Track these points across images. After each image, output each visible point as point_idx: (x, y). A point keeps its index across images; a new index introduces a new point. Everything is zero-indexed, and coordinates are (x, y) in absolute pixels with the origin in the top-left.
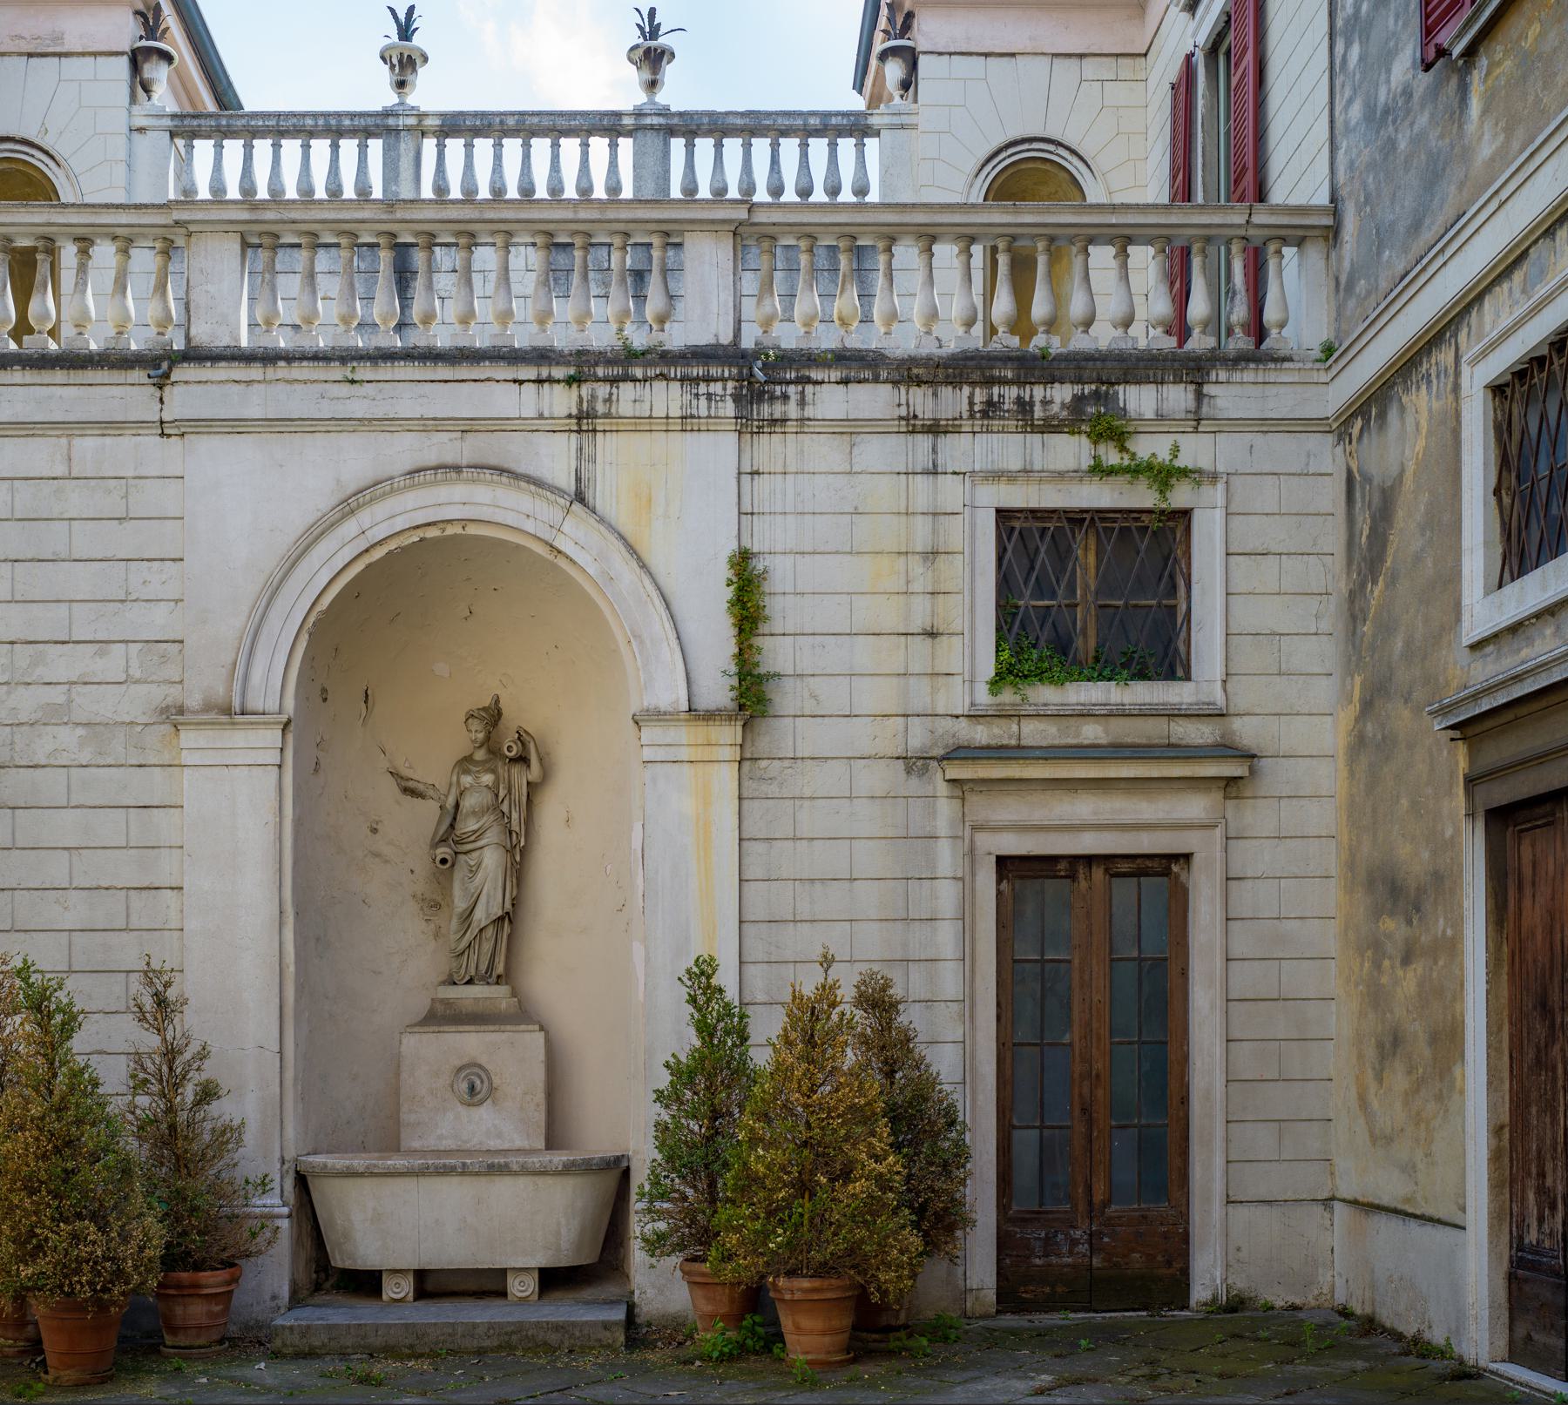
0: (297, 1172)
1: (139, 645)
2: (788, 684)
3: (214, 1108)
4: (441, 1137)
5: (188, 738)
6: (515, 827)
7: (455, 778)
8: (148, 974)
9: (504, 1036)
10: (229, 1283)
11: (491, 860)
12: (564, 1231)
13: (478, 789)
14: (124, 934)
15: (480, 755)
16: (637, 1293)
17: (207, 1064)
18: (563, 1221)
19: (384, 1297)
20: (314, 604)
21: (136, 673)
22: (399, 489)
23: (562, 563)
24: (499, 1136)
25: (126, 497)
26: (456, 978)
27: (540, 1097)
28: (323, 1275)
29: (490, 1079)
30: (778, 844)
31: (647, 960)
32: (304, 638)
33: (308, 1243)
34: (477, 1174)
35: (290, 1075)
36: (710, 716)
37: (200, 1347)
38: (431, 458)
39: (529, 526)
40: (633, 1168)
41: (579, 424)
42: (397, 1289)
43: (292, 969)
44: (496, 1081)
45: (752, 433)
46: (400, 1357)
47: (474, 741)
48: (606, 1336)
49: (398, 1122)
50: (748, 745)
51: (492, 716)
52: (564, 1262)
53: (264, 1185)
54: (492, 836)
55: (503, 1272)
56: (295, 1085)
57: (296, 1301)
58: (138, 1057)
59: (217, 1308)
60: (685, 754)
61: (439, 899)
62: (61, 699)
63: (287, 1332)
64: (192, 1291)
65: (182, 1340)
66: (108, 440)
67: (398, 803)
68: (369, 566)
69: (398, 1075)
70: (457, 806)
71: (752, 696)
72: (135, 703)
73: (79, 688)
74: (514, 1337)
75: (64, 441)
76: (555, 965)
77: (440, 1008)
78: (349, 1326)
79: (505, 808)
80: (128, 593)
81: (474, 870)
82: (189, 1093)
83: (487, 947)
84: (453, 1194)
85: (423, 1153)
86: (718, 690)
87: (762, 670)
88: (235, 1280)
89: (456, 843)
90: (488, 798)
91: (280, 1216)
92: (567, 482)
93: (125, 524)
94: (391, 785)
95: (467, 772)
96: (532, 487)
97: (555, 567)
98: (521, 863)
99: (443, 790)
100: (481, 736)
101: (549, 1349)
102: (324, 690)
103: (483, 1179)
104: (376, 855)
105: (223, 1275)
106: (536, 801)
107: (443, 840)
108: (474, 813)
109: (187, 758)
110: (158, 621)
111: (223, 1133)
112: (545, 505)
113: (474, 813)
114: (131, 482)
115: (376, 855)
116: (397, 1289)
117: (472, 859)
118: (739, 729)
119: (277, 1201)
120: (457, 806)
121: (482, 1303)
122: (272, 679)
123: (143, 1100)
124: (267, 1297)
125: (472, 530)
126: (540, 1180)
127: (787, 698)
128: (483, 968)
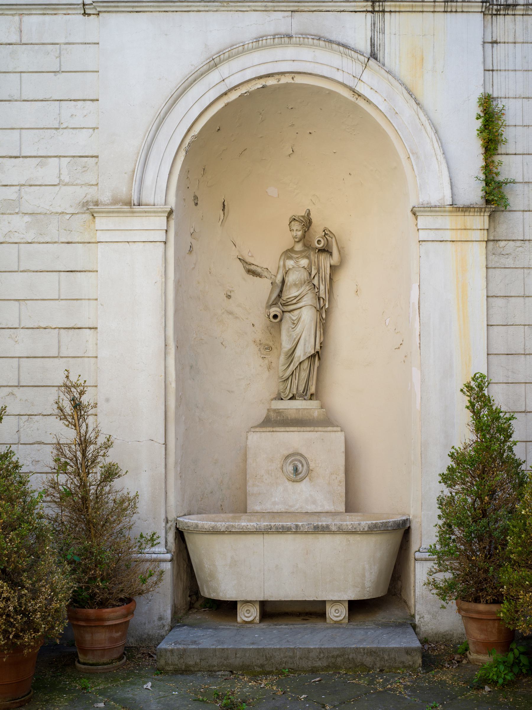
0: (177, 529)
1: (68, 159)
2: (519, 188)
3: (117, 483)
4: (274, 503)
5: (101, 222)
6: (322, 295)
7: (282, 263)
8: (67, 388)
9: (317, 434)
10: (125, 616)
11: (307, 316)
12: (367, 574)
13: (297, 270)
14: (56, 360)
15: (299, 247)
16: (417, 617)
17: (111, 451)
18: (367, 567)
19: (239, 620)
20: (189, 131)
21: (66, 178)
22: (248, 50)
23: (361, 103)
24: (314, 502)
25: (60, 56)
26: (283, 395)
27: (342, 476)
28: (194, 597)
29: (308, 464)
30: (513, 300)
31: (423, 381)
32: (182, 154)
33: (184, 576)
34: (306, 533)
35: (172, 460)
36: (466, 209)
37: (104, 664)
38: (271, 29)
39: (339, 76)
40: (413, 527)
41: (373, 6)
42: (248, 614)
43: (173, 385)
44: (312, 465)
45: (492, 15)
46: (255, 676)
47: (295, 237)
48: (408, 659)
49: (245, 494)
50: (492, 230)
51: (307, 223)
52: (366, 596)
53: (152, 540)
54: (308, 300)
55: (324, 602)
56: (175, 467)
57: (177, 621)
58: (59, 446)
59: (117, 635)
60: (448, 235)
61: (271, 344)
62: (14, 197)
63: (169, 654)
64: (97, 623)
65: (91, 659)
66: (47, 18)
67: (244, 279)
68: (227, 105)
69: (245, 460)
70: (283, 282)
71: (495, 196)
72: (66, 199)
73: (27, 189)
74: (339, 660)
75: (17, 18)
76: (347, 387)
77: (273, 415)
78: (215, 650)
79: (316, 282)
80: (60, 123)
81: (295, 324)
82: (95, 475)
83: (304, 375)
84: (287, 549)
85: (263, 514)
86: (472, 191)
87: (501, 178)
88: (130, 613)
89: (284, 305)
90: (304, 275)
91: (164, 561)
92: (365, 47)
93: (59, 75)
94: (239, 268)
95: (290, 258)
96: (341, 48)
97: (356, 107)
98: (326, 319)
99: (274, 272)
100: (300, 233)
101: (366, 668)
102: (196, 198)
103: (310, 537)
104: (230, 313)
105: (120, 610)
106: (335, 279)
107: (274, 304)
108: (295, 285)
109: (100, 236)
110: (82, 143)
111: (123, 501)
112: (350, 61)
113: (295, 285)
114: (63, 46)
115: (230, 313)
116: (248, 614)
117: (294, 316)
118: (487, 218)
119: (163, 550)
120: (283, 282)
121: (308, 625)
122: (160, 182)
123: (62, 478)
124: (156, 618)
125: (299, 80)
126: (351, 538)
127: (518, 197)
128: (301, 389)
